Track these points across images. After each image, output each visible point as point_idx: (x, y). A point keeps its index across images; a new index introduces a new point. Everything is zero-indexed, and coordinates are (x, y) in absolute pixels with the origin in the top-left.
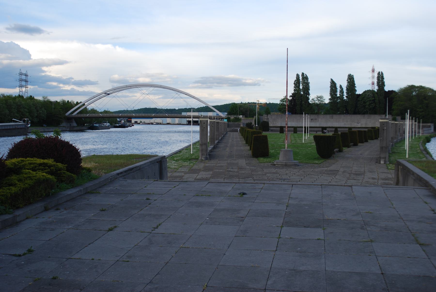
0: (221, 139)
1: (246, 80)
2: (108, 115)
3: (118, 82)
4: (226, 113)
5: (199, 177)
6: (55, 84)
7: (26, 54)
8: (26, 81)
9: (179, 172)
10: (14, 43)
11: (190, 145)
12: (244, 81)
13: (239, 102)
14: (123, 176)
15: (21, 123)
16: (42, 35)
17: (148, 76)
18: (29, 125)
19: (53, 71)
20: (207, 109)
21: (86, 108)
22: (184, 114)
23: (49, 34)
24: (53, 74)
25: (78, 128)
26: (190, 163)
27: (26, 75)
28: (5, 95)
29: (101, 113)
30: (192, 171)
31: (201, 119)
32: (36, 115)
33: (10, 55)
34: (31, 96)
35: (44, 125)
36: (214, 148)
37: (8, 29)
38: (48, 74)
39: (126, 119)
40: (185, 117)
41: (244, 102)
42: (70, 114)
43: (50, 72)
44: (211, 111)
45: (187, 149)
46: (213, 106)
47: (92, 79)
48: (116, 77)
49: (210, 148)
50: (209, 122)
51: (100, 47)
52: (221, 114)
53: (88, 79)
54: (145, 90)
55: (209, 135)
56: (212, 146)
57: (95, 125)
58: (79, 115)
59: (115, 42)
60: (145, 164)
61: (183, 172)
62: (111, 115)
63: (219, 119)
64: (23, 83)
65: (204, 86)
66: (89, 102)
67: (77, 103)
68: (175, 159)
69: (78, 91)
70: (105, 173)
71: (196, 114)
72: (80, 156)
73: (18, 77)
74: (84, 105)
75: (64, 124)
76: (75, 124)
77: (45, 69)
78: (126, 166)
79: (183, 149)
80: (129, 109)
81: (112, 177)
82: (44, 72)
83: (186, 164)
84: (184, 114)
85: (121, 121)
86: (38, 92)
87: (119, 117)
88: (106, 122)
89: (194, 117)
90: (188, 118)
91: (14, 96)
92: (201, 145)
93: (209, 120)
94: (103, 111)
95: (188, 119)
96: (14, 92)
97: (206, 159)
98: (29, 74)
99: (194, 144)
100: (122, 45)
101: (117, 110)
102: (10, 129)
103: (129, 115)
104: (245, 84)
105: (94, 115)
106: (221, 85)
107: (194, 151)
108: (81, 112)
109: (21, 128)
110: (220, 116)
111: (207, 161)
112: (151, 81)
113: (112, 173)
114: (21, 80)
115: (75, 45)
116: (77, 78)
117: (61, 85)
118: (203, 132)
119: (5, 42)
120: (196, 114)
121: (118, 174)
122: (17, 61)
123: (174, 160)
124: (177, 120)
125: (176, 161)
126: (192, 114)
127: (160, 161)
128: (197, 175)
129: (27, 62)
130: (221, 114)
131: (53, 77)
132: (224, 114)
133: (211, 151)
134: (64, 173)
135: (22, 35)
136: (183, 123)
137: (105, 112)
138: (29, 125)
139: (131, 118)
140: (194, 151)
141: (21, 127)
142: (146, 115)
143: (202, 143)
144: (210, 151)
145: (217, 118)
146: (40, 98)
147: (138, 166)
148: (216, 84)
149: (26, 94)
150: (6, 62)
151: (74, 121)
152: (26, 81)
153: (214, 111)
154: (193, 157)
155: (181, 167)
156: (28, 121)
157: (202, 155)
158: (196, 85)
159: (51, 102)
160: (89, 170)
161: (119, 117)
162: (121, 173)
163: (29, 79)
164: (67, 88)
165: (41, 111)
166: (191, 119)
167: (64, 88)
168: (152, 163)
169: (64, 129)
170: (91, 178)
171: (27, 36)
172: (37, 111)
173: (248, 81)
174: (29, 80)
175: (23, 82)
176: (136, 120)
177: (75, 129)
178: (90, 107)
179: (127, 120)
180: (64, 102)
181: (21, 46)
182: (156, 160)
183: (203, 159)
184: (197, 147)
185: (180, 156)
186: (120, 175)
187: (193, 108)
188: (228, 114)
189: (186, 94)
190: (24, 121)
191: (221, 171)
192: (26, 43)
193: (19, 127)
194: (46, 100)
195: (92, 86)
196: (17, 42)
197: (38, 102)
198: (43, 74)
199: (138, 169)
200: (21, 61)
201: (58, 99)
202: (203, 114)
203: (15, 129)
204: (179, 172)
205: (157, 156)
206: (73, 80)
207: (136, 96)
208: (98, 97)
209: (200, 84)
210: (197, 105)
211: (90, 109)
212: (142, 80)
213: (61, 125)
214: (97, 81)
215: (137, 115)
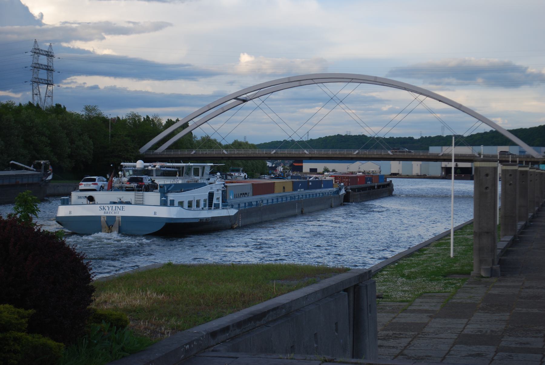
0: (533, 217)
2: (242, 152)
5: (471, 329)
8: (49, 69)
9: (414, 311)
11: (448, 234)
14: (232, 339)
15: (31, 171)
18: (50, 177)
20: (494, 137)
21: (190, 133)
22: (434, 150)
26: (446, 286)
27: (49, 55)
29: (227, 147)
30: (452, 310)
31: (478, 164)
32: (69, 150)
34: (58, 106)
36: (514, 243)
39: (288, 163)
40: (436, 159)
42: (150, 149)
44: (507, 142)
45: (440, 245)
49: (503, 242)
50: (499, 171)
52: (530, 151)
55: (499, 204)
56: (509, 238)
60: (306, 297)
61: (426, 311)
62: (250, 152)
63: (527, 163)
64: (43, 75)
67: (170, 123)
68: (406, 272)
70: (175, 329)
71: (466, 150)
72: (88, 278)
74: (185, 125)
78: (246, 304)
79: (428, 244)
80: (297, 139)
81: (189, 344)
83: (436, 286)
84: (434, 150)
85: (274, 169)
87: (270, 158)
88: (238, 171)
89: (459, 159)
90: (445, 160)
91: (17, 104)
92: (478, 235)
93: (500, 168)
94: (230, 142)
95: (444, 164)
96: (19, 97)
97: (492, 273)
99: (459, 230)
103: (294, 152)
107: (460, 248)
108: (176, 146)
110: (528, 156)
111: (494, 280)
113: (195, 330)
114: (37, 67)
118: (483, 199)
120: (466, 150)
121: (214, 334)
123: (403, 276)
124: (416, 167)
125: (409, 277)
126: (453, 150)
127: (355, 286)
128: (465, 321)
130: (530, 151)
132: (539, 152)
133: (506, 252)
134: (16, 339)
136: (432, 173)
137: (237, 145)
138: (50, 177)
139: (301, 159)
140: (460, 248)
141: (30, 181)
142: (337, 152)
143: (478, 231)
144: (502, 250)
145: (527, 163)
147: (283, 306)
149: (49, 100)
152: (47, 70)
154: (456, 267)
155: (420, 296)
156: (46, 168)
157: (481, 262)
159: (105, 121)
160: (118, 323)
161: (270, 158)
162: (225, 329)
163: (56, 64)
166: (452, 165)
168: (329, 293)
170: (123, 349)
175: (41, 71)
176: (313, 165)
178: (199, 134)
179: (291, 165)
180: (135, 118)
182: (342, 283)
183: (483, 274)
184: (467, 240)
185: (418, 264)
186: (221, 337)
187: (457, 137)
190: (38, 167)
191: (536, 311)
193: (25, 181)
194: (93, 114)
197: (75, 119)
199: (286, 313)
201: (122, 114)
202: (484, 150)
204: (414, 311)
205: (346, 270)
208: (219, 106)
210: (469, 127)
211: (199, 138)
215: (316, 152)
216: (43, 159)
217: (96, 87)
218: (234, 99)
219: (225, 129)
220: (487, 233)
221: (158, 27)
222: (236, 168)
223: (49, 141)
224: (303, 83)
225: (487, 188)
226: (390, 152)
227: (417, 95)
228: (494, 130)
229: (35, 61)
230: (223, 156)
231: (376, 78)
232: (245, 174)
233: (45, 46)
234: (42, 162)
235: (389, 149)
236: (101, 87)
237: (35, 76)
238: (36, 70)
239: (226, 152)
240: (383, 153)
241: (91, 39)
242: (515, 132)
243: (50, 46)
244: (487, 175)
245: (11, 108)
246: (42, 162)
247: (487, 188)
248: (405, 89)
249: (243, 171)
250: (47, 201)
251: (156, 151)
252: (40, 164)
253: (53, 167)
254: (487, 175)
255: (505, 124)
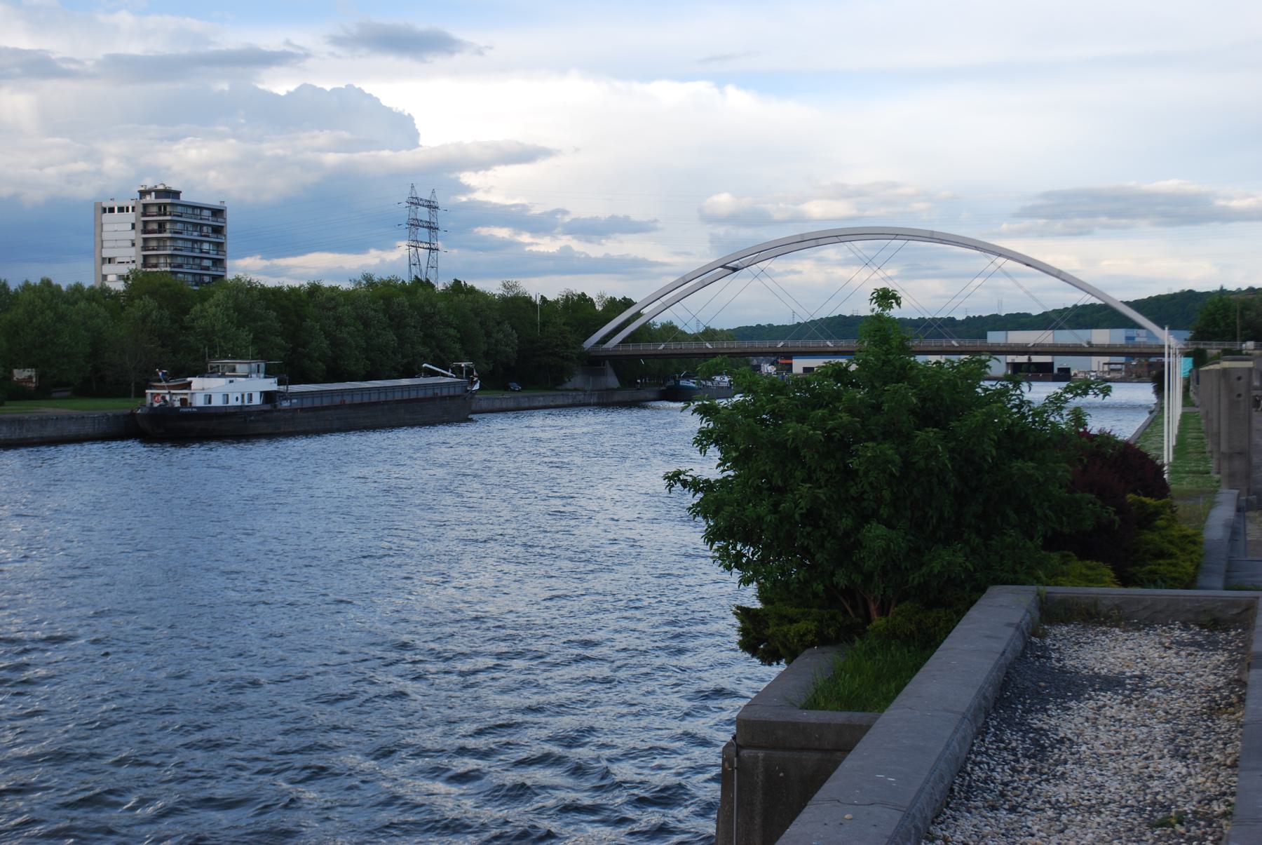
1: (1231, 198)
3: (734, 219)
4: (1187, 334)
6: (502, 233)
7: (403, 128)
8: (432, 228)
10: (360, 90)
12: (1221, 203)
13: (1213, 287)
15: (449, 378)
16: (458, 58)
17: (843, 193)
18: (477, 387)
19: (493, 187)
20: (1099, 315)
23: (480, 52)
24: (496, 198)
25: (626, 395)
27: (432, 206)
28: (376, 279)
29: (696, 338)
33: (346, 135)
35: (514, 385)
37: (338, 41)
38: (479, 196)
41: (1231, 286)
43: (488, 191)
46: (1127, 303)
47: (637, 214)
48: (723, 201)
51: (668, 93)
53: (620, 213)
54: (831, 252)
57: (683, 383)
58: (631, 349)
59: (719, 69)
65: (1059, 225)
66: (663, 299)
69: (588, 258)
73: (404, 213)
75: (577, 381)
76: (612, 381)
77: (468, 178)
82: (467, 189)
84: (995, 337)
86: (461, 265)
98: (441, 201)
100: (747, 81)
101: (1164, 292)
102: (417, 400)
104: (1227, 216)
105: (673, 347)
106: (1124, 221)
108: (633, 338)
109: (452, 397)
112: (854, 212)
114: (415, 224)
115: (579, 92)
116: (584, 208)
117: (525, 238)
119: (328, 87)
122: (373, 153)
129: (404, 158)
131: (495, 204)
135: (389, 61)
138: (477, 387)
146: (492, 286)
148: (1104, 220)
150: (331, 159)
151: (610, 371)
152: (430, 228)
153: (1140, 327)
158: (1027, 223)
159: (528, 301)
163: (442, 220)
164: (547, 245)
165: (501, 336)
167: (534, 249)
169: (581, 397)
171: (405, 63)
172: (488, 334)
173: (1236, 204)
174: (440, 226)
177: (617, 397)
181: (386, 101)
188: (1193, 339)
189: (1029, 263)
190: (458, 371)
192: (397, 88)
195: (636, 236)
196: (369, 87)
198: (464, 199)
200: (386, 153)
203: (433, 399)
206: (567, 219)
207: (800, 272)
208: (703, 278)
209: (1041, 222)
212: (822, 212)
213: (569, 385)
214: (656, 221)
219: (700, 312)
220: (1240, 454)
224: (821, 241)
225: (1239, 395)
226: (954, 343)
227: (993, 257)
228: (1099, 302)
229: (413, 216)
233: (424, 195)
235: (952, 338)
238: (413, 229)
240: (944, 343)
242: (1137, 305)
244: (1239, 378)
245: (395, 287)
247: (1239, 395)
250: (471, 420)
251: (606, 346)
254: (1239, 378)
255: (1120, 295)
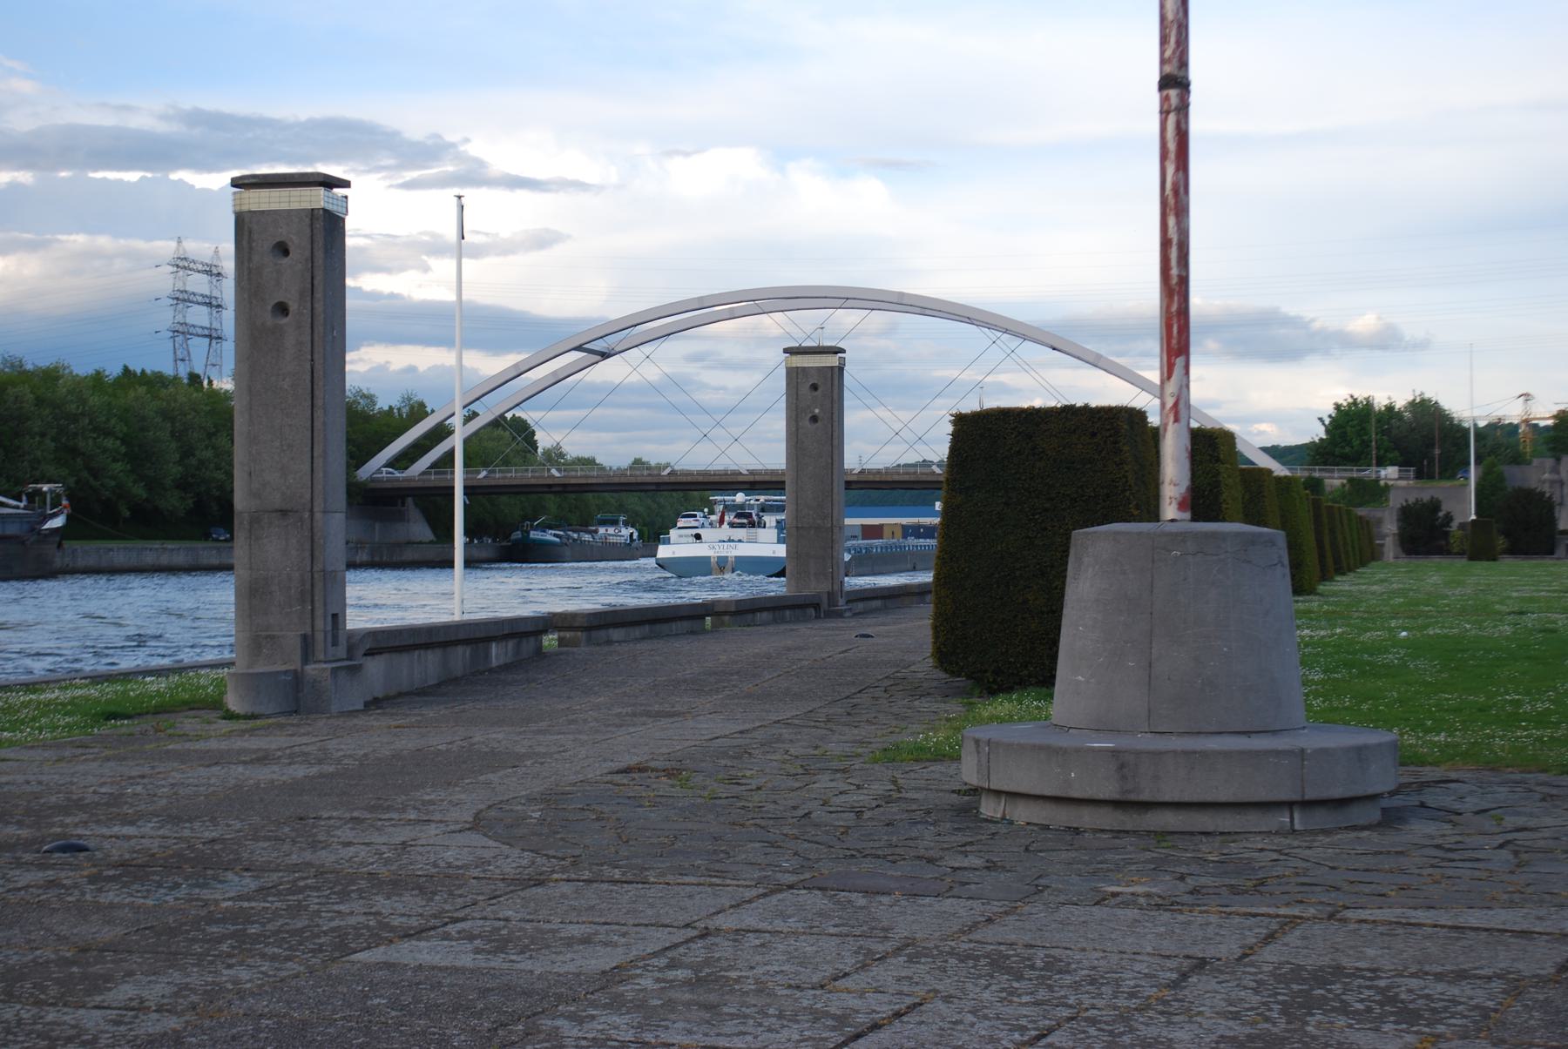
88: (614, 523)
216: (49, 482)
217: (411, 370)
218: (579, 348)
220: (284, 513)
221: (542, 241)
222: (609, 516)
223: (123, 449)
230: (550, 482)
231: (902, 294)
232: (631, 530)
234: (45, 488)
236: (422, 368)
237: (179, 318)
239: (557, 474)
241: (402, 269)
243: (216, 252)
246: (45, 488)
248: (970, 321)
249: (626, 524)
252: (39, 492)
253: (69, 498)
